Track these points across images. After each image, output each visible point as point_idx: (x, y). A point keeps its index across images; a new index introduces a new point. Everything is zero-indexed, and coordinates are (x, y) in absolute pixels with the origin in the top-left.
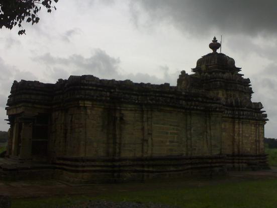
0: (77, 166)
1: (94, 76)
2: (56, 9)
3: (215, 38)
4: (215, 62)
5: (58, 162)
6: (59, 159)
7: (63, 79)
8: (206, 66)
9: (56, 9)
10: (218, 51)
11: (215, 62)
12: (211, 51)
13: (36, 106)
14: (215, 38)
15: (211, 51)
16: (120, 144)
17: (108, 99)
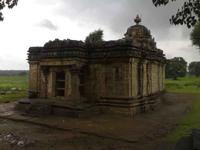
0: (107, 102)
1: (61, 39)
2: (179, 10)
3: (138, 16)
4: (141, 31)
5: (101, 100)
6: (101, 98)
7: (59, 40)
8: (136, 33)
9: (179, 10)
10: (139, 24)
11: (141, 31)
12: (135, 24)
13: (82, 60)
14: (138, 16)
15: (135, 24)
16: (142, 87)
17: (83, 56)
